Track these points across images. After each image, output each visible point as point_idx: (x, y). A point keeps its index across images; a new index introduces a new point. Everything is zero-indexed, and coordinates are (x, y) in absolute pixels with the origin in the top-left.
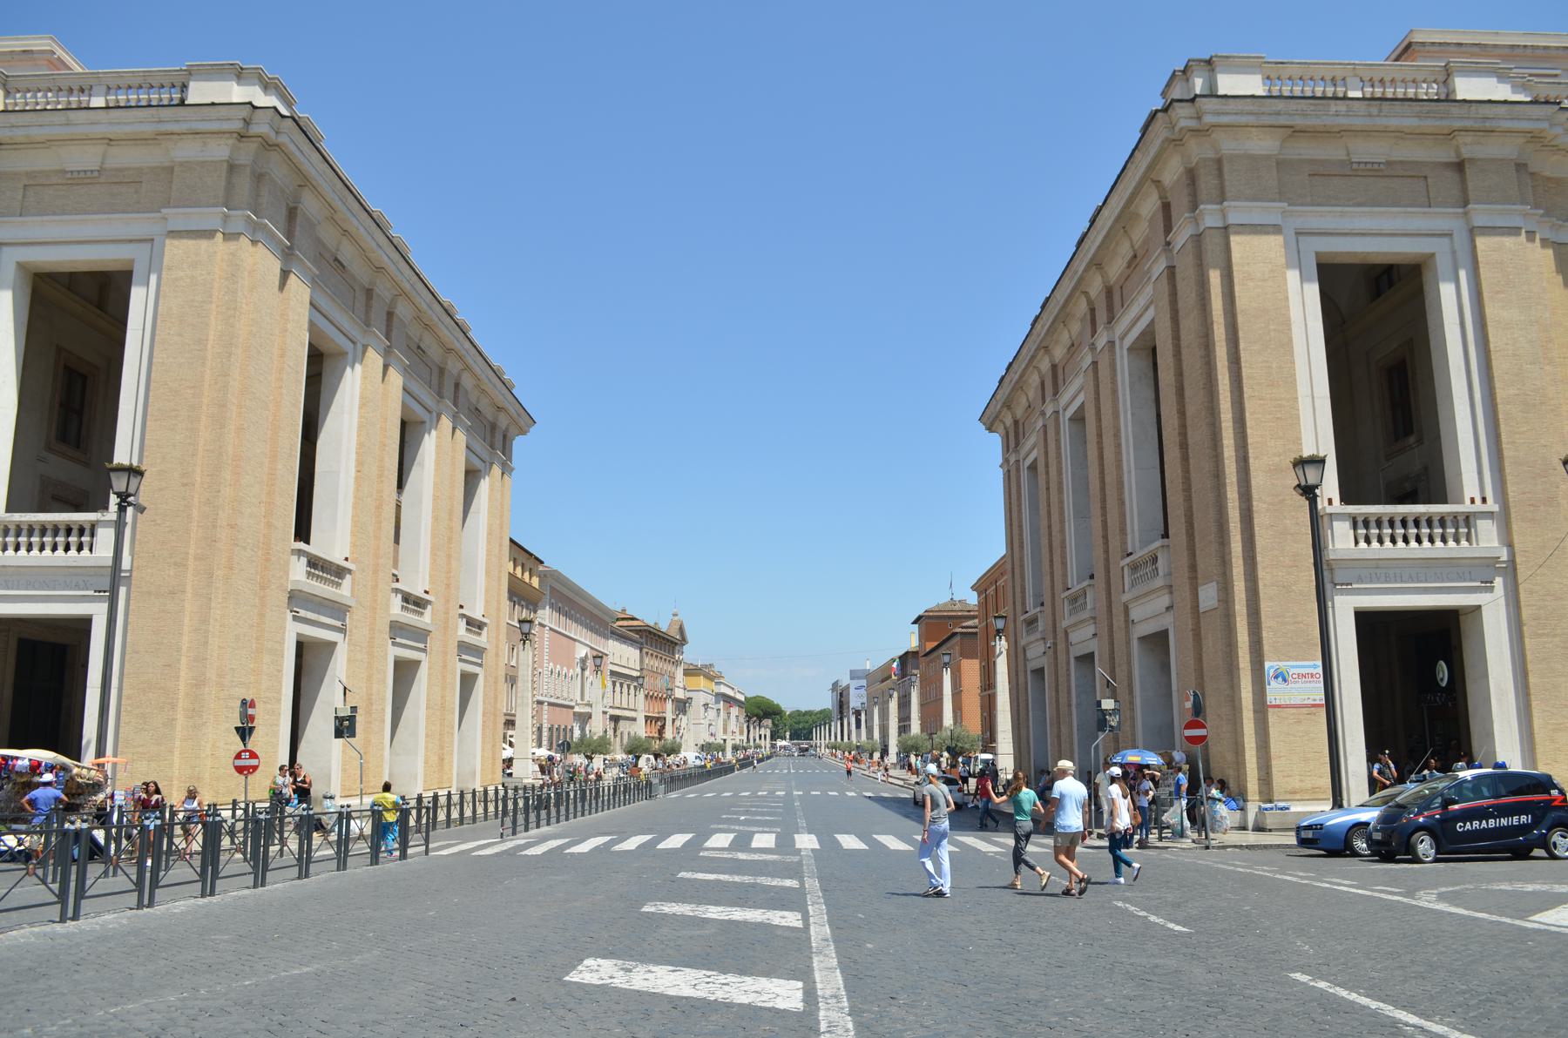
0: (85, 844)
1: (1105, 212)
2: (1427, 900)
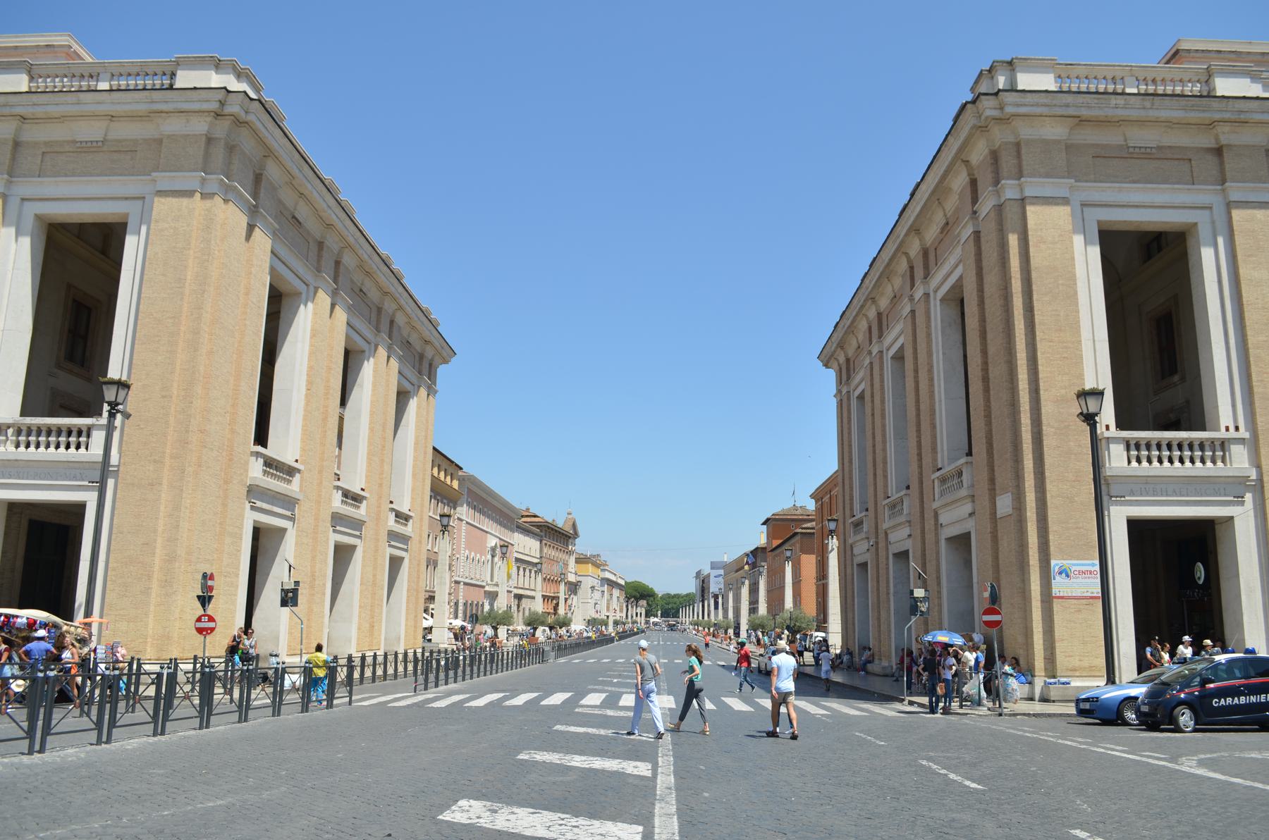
0: (57, 690)
1: (923, 187)
2: (1189, 765)
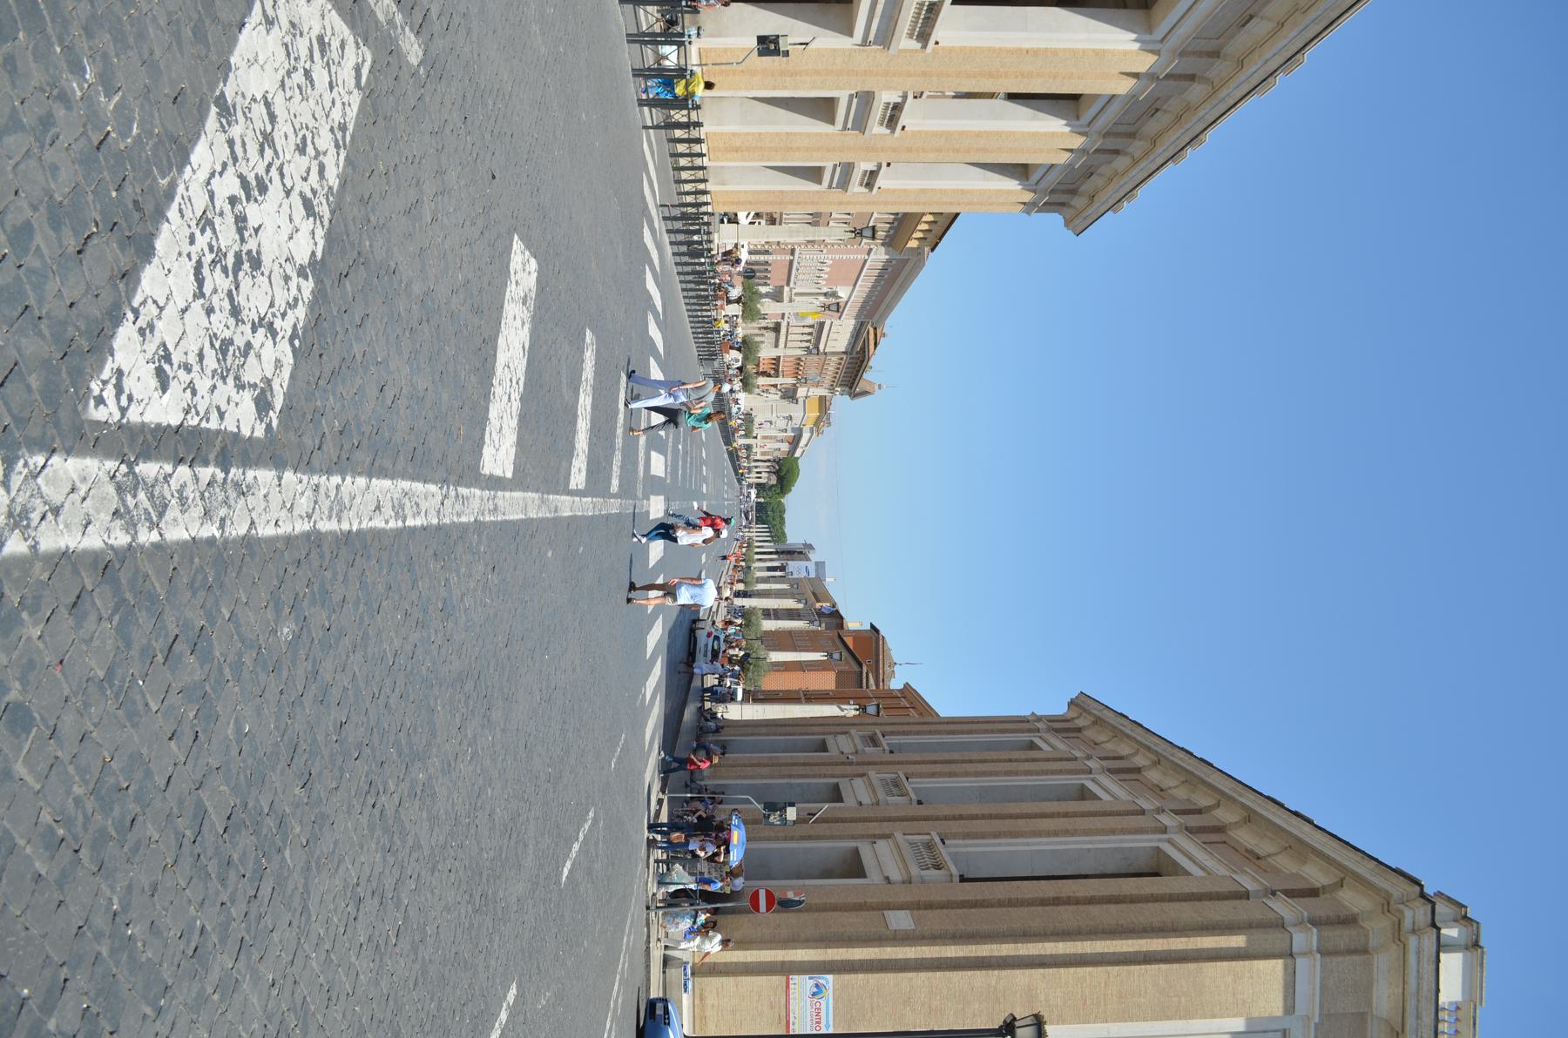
1: (1307, 827)
